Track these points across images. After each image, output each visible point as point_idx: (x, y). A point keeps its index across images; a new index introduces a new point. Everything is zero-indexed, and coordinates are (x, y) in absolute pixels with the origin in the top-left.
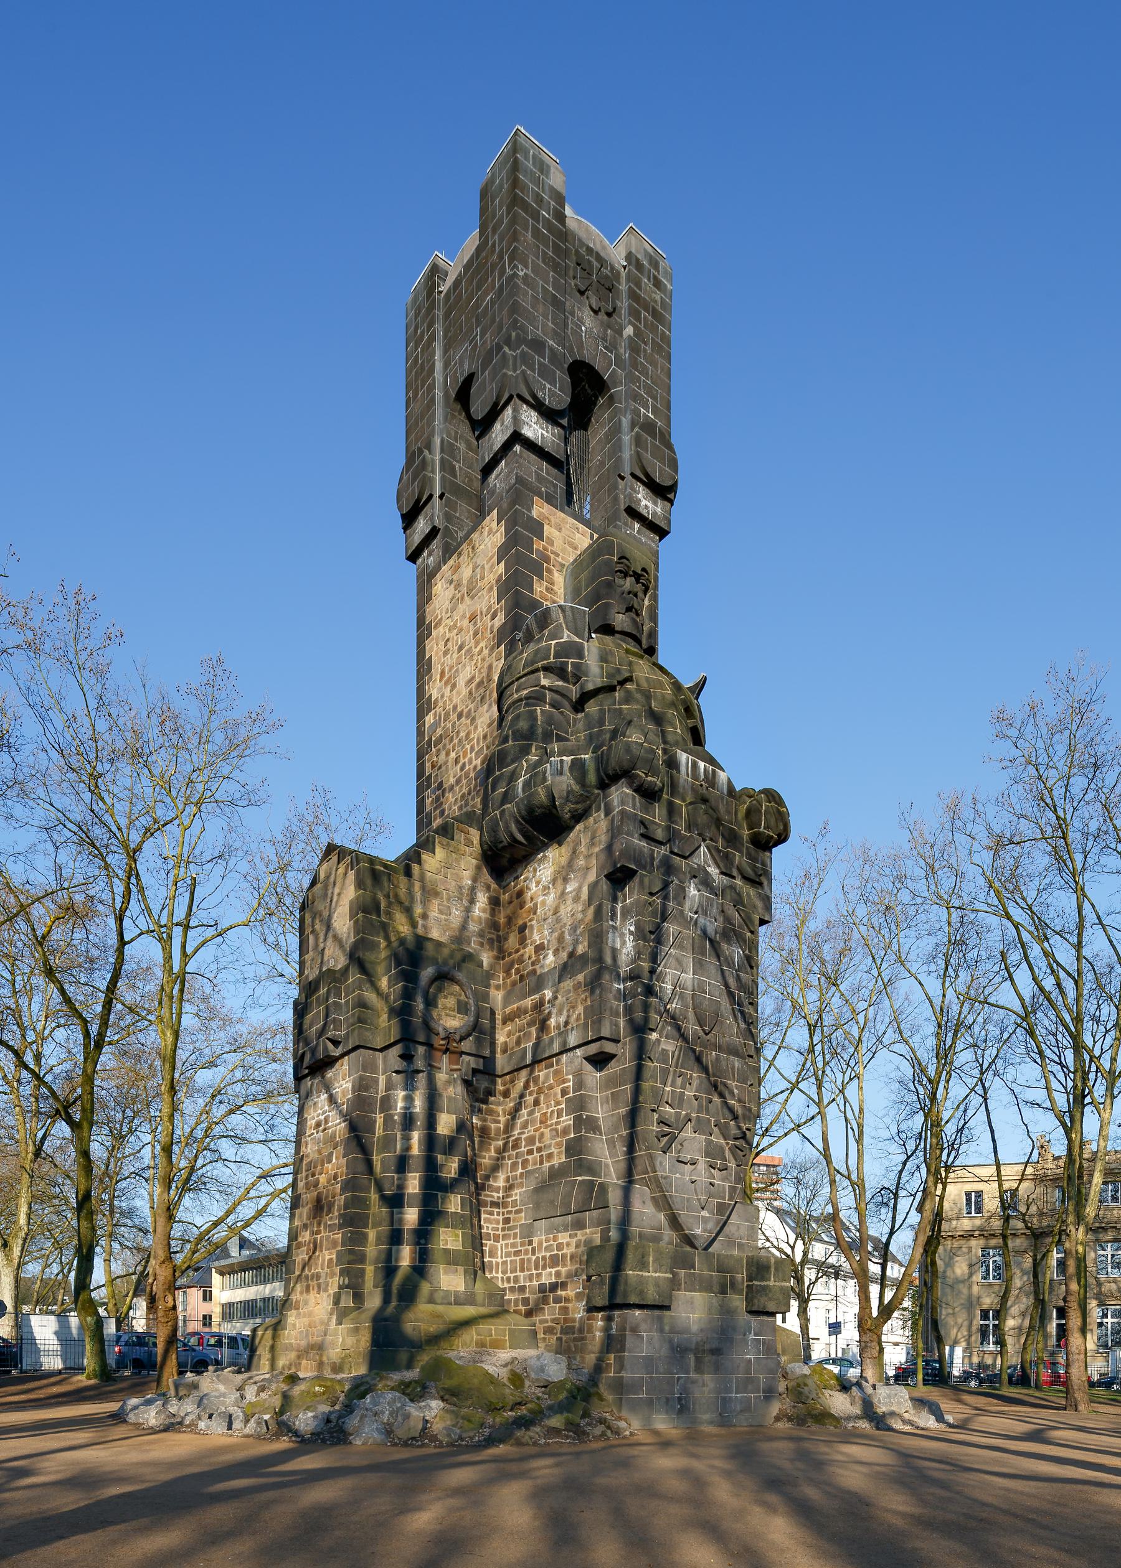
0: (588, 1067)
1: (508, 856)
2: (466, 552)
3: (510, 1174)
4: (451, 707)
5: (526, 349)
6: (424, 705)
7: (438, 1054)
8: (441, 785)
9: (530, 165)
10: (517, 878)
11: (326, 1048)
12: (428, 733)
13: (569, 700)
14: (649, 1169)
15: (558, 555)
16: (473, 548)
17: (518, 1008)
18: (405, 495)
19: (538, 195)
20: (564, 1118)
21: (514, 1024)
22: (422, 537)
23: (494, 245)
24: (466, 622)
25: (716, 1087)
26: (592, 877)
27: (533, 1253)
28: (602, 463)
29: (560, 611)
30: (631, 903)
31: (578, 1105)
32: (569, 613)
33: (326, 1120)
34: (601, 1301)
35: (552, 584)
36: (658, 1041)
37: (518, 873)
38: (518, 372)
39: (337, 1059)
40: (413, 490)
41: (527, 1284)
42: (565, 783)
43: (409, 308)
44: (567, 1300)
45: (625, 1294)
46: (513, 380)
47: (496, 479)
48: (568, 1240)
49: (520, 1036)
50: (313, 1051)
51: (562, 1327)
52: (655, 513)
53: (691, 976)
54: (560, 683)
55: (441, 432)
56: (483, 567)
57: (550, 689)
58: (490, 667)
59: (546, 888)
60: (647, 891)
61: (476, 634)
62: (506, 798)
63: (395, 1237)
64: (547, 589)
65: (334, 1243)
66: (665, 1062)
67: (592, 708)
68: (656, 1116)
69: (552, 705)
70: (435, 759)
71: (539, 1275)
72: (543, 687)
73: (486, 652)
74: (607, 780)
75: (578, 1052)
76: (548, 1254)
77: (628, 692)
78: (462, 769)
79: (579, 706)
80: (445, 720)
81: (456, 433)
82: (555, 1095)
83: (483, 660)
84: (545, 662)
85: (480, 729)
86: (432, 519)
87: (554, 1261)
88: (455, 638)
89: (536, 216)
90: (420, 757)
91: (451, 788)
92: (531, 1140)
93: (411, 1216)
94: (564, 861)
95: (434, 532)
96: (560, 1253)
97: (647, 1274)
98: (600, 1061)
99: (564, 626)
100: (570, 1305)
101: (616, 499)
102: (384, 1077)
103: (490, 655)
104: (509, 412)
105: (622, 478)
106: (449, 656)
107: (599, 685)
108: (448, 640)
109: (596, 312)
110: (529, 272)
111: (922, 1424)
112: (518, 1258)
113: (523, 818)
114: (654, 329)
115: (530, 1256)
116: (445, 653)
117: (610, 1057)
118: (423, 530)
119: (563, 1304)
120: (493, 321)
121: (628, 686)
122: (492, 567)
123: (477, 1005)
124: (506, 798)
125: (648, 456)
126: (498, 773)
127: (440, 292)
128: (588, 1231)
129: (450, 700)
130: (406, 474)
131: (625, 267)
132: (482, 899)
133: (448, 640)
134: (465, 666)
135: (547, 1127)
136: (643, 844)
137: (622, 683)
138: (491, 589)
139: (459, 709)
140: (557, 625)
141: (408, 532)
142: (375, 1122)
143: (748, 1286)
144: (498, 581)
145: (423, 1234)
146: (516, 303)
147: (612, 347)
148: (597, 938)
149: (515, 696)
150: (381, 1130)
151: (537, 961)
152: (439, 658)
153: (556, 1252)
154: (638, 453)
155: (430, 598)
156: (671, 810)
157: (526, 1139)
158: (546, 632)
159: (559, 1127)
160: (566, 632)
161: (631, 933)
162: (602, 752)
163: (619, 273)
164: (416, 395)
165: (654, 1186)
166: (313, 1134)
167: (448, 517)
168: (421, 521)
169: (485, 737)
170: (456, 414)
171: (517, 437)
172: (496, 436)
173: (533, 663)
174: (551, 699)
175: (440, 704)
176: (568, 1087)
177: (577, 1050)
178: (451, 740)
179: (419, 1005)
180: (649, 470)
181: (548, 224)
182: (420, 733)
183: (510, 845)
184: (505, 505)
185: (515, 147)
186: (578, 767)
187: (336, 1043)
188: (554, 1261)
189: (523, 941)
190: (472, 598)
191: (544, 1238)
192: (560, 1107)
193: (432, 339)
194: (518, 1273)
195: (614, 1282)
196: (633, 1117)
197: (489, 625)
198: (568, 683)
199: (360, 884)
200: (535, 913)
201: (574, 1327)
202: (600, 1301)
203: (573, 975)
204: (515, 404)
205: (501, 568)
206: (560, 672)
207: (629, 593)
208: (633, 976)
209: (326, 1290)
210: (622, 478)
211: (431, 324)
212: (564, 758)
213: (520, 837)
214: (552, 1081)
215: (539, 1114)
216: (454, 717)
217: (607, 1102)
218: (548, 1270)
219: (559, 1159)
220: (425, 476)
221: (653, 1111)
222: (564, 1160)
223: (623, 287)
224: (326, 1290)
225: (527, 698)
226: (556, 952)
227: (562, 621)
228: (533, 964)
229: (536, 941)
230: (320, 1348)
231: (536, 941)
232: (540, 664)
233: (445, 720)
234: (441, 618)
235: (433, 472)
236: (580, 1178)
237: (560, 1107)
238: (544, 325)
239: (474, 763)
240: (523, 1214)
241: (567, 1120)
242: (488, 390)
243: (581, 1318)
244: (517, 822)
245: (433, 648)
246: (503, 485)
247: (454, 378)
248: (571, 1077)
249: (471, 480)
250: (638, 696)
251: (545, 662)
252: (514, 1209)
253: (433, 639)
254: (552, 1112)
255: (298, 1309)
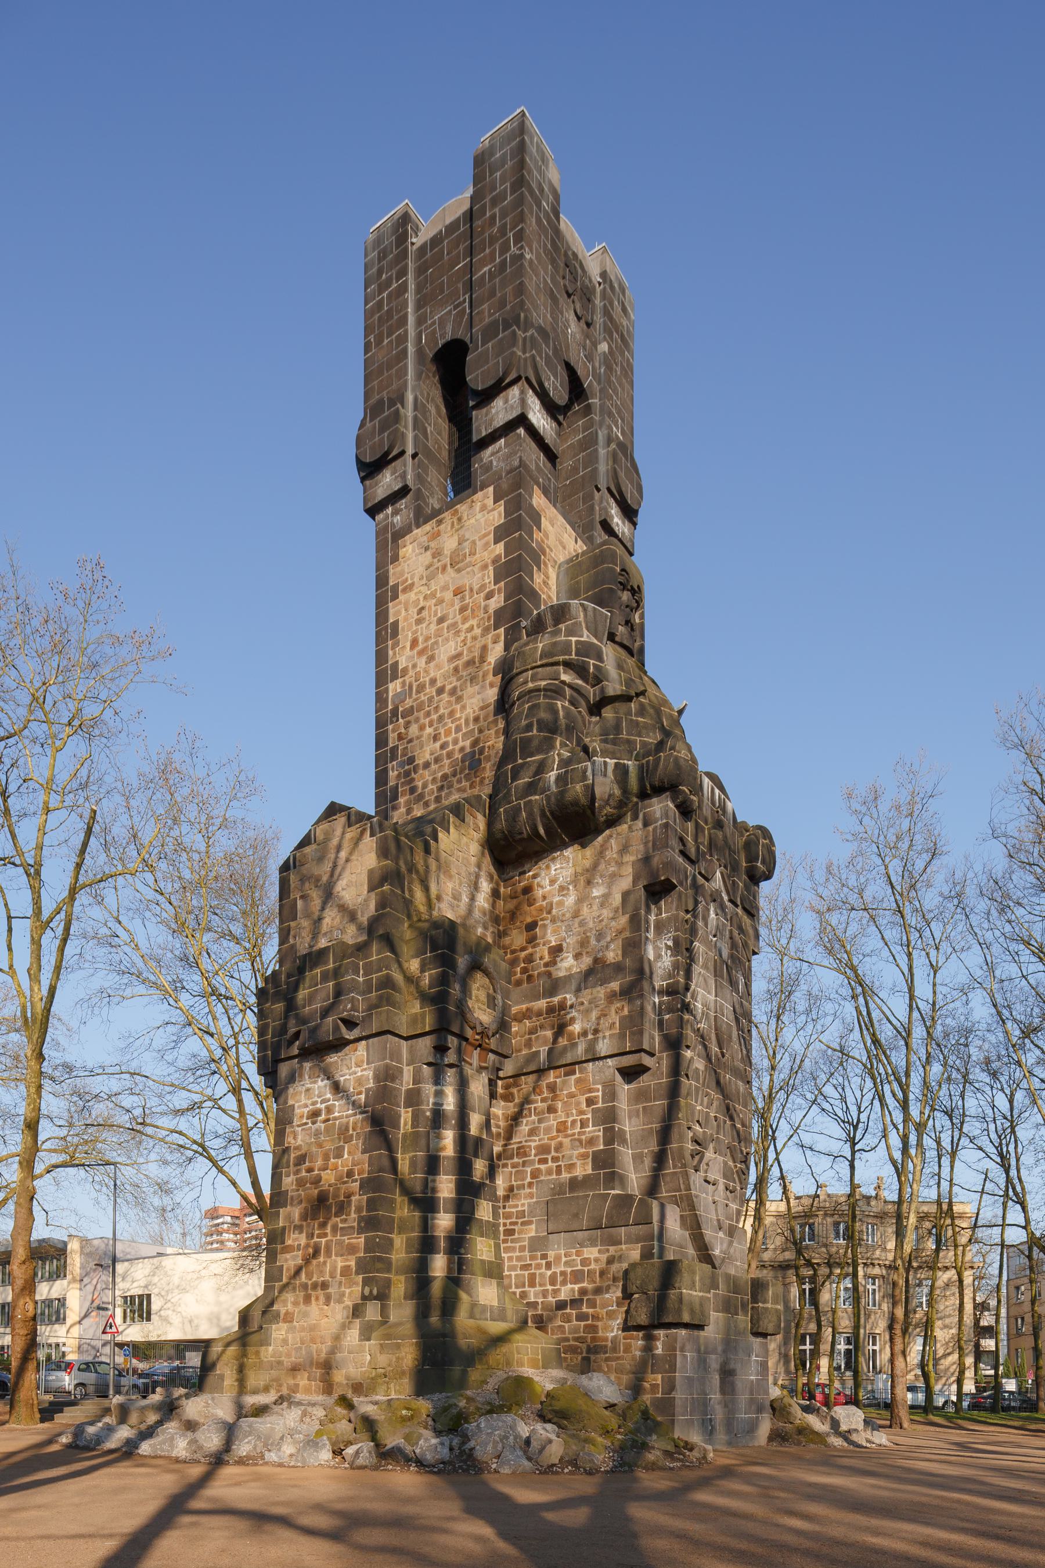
0: (618, 1078)
1: (520, 848)
2: (450, 522)
3: (514, 1183)
4: (427, 679)
5: (536, 335)
6: (385, 673)
7: (470, 1048)
8: (411, 760)
9: (534, 150)
10: (524, 873)
11: (336, 1028)
12: (393, 702)
13: (587, 701)
14: (682, 1187)
15: (551, 550)
16: (460, 519)
17: (528, 1009)
18: (369, 443)
19: (540, 184)
20: (590, 1129)
21: (522, 1025)
22: (389, 492)
23: (493, 217)
24: (448, 595)
25: (728, 1109)
26: (625, 883)
27: (548, 1266)
28: (575, 470)
29: (581, 609)
30: (668, 918)
31: (608, 1118)
32: (590, 613)
33: (329, 1110)
34: (642, 1317)
35: (548, 578)
36: (691, 1060)
37: (526, 868)
38: (528, 355)
39: (348, 1042)
40: (382, 441)
41: (540, 1301)
42: (605, 787)
43: (369, 248)
44: (595, 1317)
45: (679, 1311)
46: (522, 361)
47: (493, 454)
48: (597, 1255)
49: (530, 1039)
50: (314, 1031)
51: (588, 1346)
52: (623, 533)
53: (713, 998)
54: (580, 682)
55: (413, 390)
56: (474, 542)
57: (570, 686)
58: (484, 649)
59: (562, 888)
60: (684, 907)
61: (463, 609)
62: (532, 788)
63: (427, 1245)
64: (544, 582)
65: (352, 1249)
66: (698, 1081)
67: (608, 713)
68: (691, 1134)
69: (572, 703)
70: (403, 731)
71: (556, 1292)
72: (563, 682)
73: (477, 631)
74: (650, 790)
75: (610, 1062)
76: (569, 1270)
77: (642, 705)
78: (442, 747)
79: (596, 709)
80: (418, 692)
81: (428, 394)
82: (578, 1104)
83: (474, 638)
84: (567, 657)
85: (469, 710)
86: (403, 476)
87: (577, 1277)
88: (433, 608)
89: (539, 205)
90: (381, 723)
91: (427, 765)
92: (544, 1149)
93: (444, 1221)
94: (587, 863)
95: (404, 491)
96: (586, 1269)
97: (695, 1293)
98: (630, 1074)
99: (584, 625)
100: (600, 1324)
101: (592, 508)
102: (411, 1068)
103: (483, 635)
104: (514, 392)
105: (598, 490)
106: (424, 625)
107: (619, 693)
108: (423, 608)
109: (579, 318)
110: (534, 258)
111: (877, 1441)
112: (526, 1273)
113: (552, 813)
114: (622, 354)
115: (543, 1270)
116: (419, 622)
117: (643, 1069)
118: (389, 486)
119: (590, 1322)
120: (492, 294)
121: (642, 699)
122: (487, 544)
123: (504, 1003)
124: (532, 788)
125: (622, 475)
126: (520, 761)
127: (413, 244)
128: (624, 1247)
129: (426, 671)
130: (371, 421)
131: (600, 284)
132: (485, 886)
133: (423, 608)
134: (447, 640)
135: (566, 1136)
136: (681, 860)
137: (638, 695)
138: (485, 567)
139: (439, 684)
140: (576, 623)
141: (367, 483)
142: (400, 1116)
143: (753, 1308)
144: (494, 562)
145: (457, 1243)
146: (522, 284)
147: (590, 357)
148: (633, 945)
149: (531, 685)
150: (409, 1126)
151: (553, 963)
152: (410, 626)
153: (579, 1267)
154: (615, 470)
155: (395, 558)
156: (698, 828)
157: (536, 1148)
158: (562, 626)
159: (583, 1137)
160: (585, 632)
161: (668, 947)
162: (648, 762)
163: (594, 287)
164: (379, 341)
165: (685, 1204)
166: (306, 1124)
167: (419, 478)
168: (388, 475)
169: (476, 719)
170: (431, 375)
171: (522, 420)
172: (497, 413)
173: (552, 655)
174: (571, 696)
175: (411, 673)
176: (596, 1097)
177: (609, 1060)
178: (428, 714)
179: (455, 990)
180: (623, 489)
181: (546, 213)
182: (381, 699)
183: (530, 838)
184: (505, 486)
185: (521, 128)
186: (621, 772)
187: (350, 1024)
188: (577, 1277)
189: (532, 940)
190: (459, 571)
191: (563, 1252)
192: (585, 1117)
193: (403, 289)
194: (527, 1289)
195: (662, 1299)
196: (665, 1134)
197: (483, 604)
198: (587, 683)
199: (383, 852)
200: (549, 912)
201: (606, 1346)
202: (643, 1318)
203: (604, 982)
204: (523, 385)
205: (500, 548)
206: (580, 670)
207: (627, 606)
208: (671, 991)
209: (340, 1301)
210: (598, 490)
211: (403, 272)
212: (607, 760)
213: (542, 831)
214: (573, 1089)
215: (555, 1123)
216: (430, 691)
217: (638, 1116)
218: (569, 1286)
219: (584, 1169)
220: (397, 430)
221: (689, 1128)
222: (590, 1171)
223: (598, 301)
224: (340, 1301)
225: (545, 689)
226: (577, 956)
227: (581, 618)
228: (546, 965)
229: (550, 942)
230: (327, 1366)
231: (550, 942)
232: (561, 658)
233: (418, 692)
234: (413, 584)
235: (406, 427)
236: (613, 1192)
237: (585, 1117)
238: (545, 316)
239: (461, 744)
240: (533, 1226)
241: (594, 1131)
242: (491, 363)
243: (615, 1337)
244: (543, 814)
245: (398, 611)
246: (503, 465)
247: (432, 337)
248: (600, 1087)
249: (440, 448)
250: (651, 711)
251: (567, 657)
252: (520, 1221)
253: (400, 603)
254: (574, 1122)
255: (291, 1321)
